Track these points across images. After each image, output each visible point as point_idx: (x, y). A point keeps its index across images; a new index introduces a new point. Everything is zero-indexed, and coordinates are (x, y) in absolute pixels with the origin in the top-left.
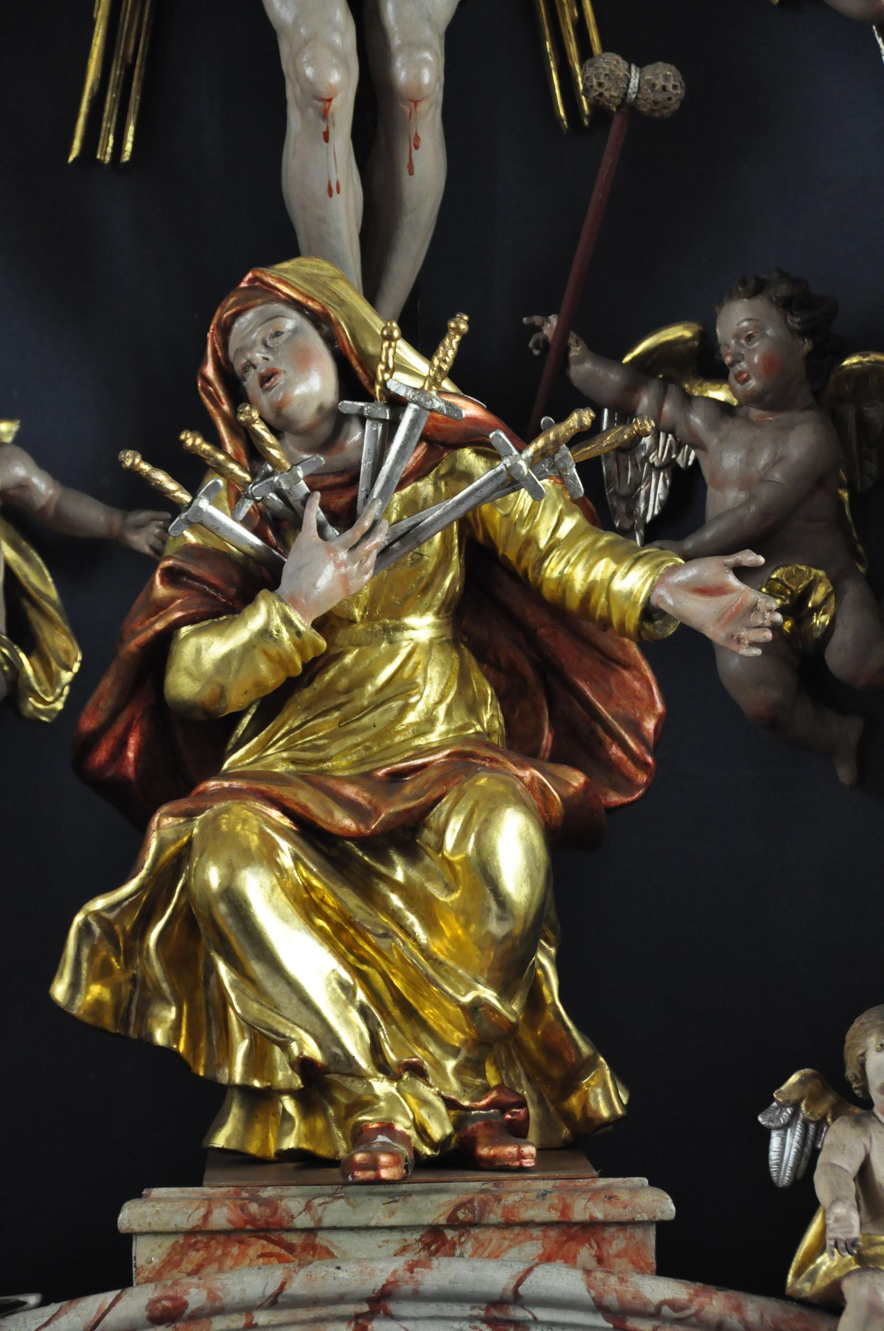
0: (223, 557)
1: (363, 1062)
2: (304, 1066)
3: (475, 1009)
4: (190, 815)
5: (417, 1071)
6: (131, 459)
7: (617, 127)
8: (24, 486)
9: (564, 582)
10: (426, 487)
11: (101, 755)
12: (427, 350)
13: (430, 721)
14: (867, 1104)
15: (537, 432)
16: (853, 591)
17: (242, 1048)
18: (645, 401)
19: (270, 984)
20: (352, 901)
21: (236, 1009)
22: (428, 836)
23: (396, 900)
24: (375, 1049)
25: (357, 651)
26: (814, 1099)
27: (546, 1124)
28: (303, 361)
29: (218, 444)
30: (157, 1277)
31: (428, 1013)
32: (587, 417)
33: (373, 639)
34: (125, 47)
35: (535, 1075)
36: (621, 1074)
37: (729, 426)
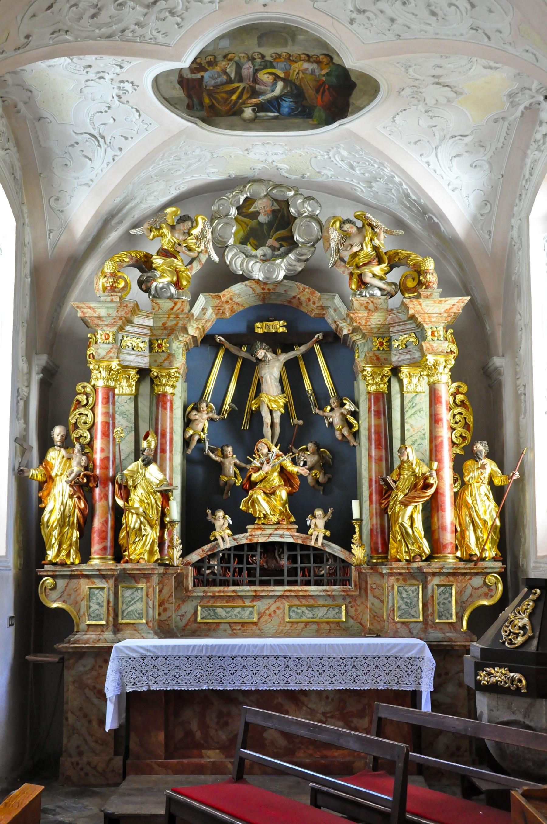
1: (269, 514)
2: (264, 514)
3: (280, 509)
5: (274, 515)
6: (248, 457)
10: (276, 460)
11: (245, 486)
17: (258, 513)
18: (300, 454)
20: (268, 499)
28: (264, 448)
34: (248, 417)
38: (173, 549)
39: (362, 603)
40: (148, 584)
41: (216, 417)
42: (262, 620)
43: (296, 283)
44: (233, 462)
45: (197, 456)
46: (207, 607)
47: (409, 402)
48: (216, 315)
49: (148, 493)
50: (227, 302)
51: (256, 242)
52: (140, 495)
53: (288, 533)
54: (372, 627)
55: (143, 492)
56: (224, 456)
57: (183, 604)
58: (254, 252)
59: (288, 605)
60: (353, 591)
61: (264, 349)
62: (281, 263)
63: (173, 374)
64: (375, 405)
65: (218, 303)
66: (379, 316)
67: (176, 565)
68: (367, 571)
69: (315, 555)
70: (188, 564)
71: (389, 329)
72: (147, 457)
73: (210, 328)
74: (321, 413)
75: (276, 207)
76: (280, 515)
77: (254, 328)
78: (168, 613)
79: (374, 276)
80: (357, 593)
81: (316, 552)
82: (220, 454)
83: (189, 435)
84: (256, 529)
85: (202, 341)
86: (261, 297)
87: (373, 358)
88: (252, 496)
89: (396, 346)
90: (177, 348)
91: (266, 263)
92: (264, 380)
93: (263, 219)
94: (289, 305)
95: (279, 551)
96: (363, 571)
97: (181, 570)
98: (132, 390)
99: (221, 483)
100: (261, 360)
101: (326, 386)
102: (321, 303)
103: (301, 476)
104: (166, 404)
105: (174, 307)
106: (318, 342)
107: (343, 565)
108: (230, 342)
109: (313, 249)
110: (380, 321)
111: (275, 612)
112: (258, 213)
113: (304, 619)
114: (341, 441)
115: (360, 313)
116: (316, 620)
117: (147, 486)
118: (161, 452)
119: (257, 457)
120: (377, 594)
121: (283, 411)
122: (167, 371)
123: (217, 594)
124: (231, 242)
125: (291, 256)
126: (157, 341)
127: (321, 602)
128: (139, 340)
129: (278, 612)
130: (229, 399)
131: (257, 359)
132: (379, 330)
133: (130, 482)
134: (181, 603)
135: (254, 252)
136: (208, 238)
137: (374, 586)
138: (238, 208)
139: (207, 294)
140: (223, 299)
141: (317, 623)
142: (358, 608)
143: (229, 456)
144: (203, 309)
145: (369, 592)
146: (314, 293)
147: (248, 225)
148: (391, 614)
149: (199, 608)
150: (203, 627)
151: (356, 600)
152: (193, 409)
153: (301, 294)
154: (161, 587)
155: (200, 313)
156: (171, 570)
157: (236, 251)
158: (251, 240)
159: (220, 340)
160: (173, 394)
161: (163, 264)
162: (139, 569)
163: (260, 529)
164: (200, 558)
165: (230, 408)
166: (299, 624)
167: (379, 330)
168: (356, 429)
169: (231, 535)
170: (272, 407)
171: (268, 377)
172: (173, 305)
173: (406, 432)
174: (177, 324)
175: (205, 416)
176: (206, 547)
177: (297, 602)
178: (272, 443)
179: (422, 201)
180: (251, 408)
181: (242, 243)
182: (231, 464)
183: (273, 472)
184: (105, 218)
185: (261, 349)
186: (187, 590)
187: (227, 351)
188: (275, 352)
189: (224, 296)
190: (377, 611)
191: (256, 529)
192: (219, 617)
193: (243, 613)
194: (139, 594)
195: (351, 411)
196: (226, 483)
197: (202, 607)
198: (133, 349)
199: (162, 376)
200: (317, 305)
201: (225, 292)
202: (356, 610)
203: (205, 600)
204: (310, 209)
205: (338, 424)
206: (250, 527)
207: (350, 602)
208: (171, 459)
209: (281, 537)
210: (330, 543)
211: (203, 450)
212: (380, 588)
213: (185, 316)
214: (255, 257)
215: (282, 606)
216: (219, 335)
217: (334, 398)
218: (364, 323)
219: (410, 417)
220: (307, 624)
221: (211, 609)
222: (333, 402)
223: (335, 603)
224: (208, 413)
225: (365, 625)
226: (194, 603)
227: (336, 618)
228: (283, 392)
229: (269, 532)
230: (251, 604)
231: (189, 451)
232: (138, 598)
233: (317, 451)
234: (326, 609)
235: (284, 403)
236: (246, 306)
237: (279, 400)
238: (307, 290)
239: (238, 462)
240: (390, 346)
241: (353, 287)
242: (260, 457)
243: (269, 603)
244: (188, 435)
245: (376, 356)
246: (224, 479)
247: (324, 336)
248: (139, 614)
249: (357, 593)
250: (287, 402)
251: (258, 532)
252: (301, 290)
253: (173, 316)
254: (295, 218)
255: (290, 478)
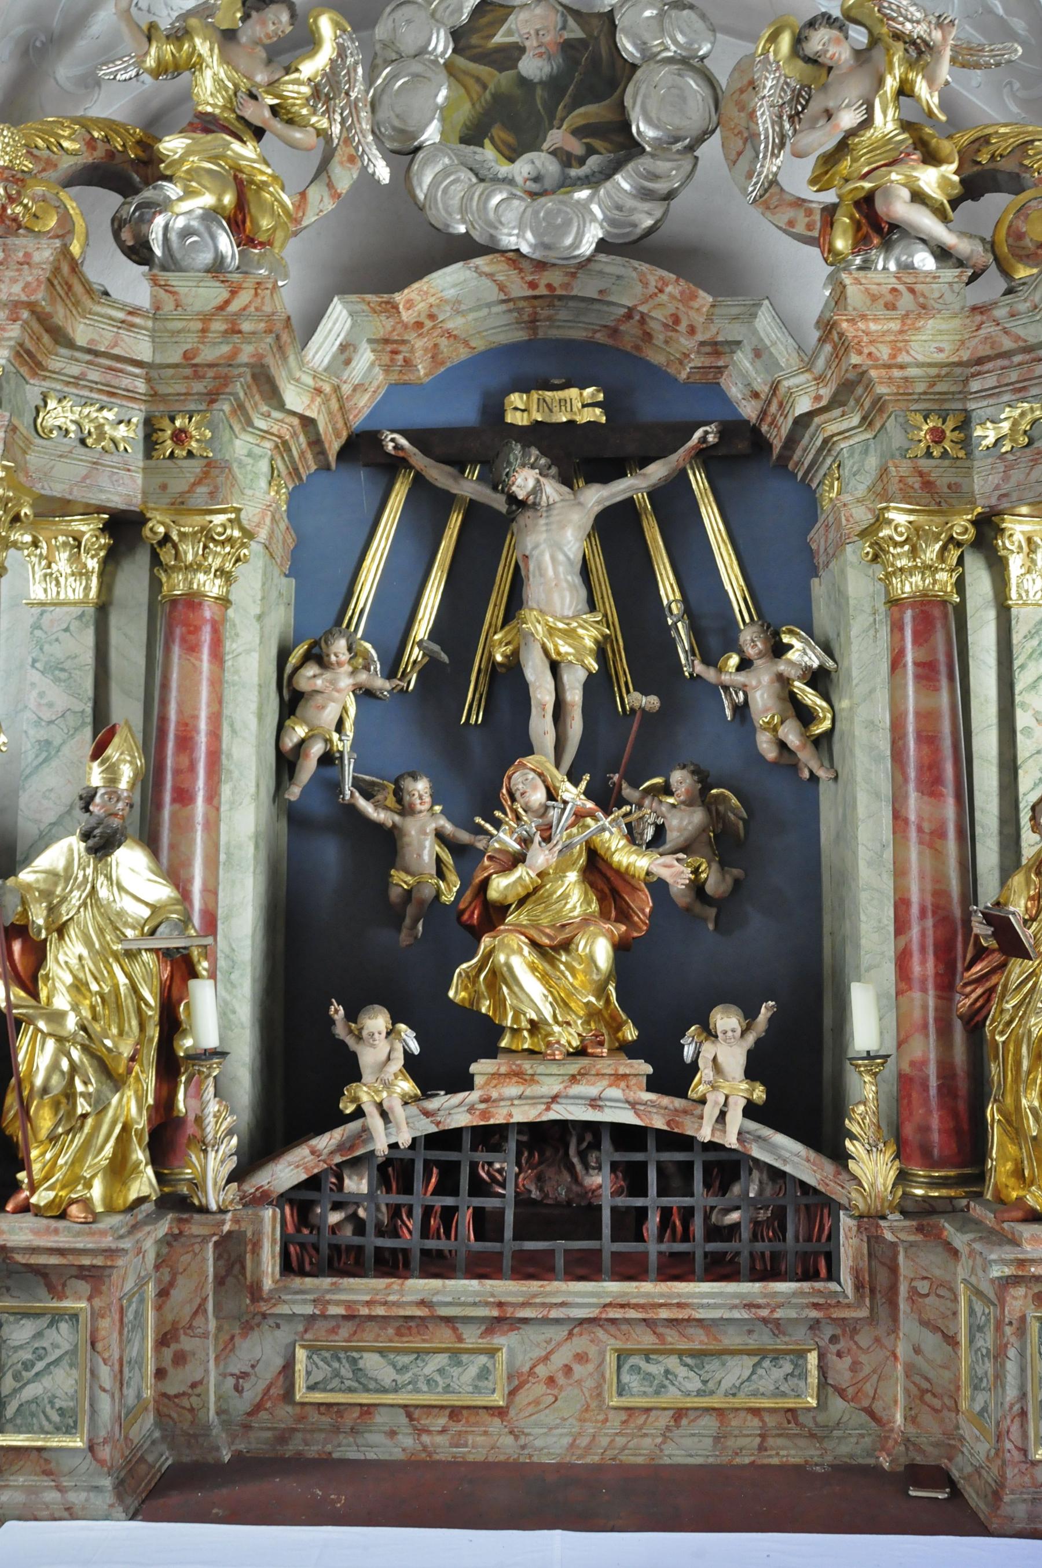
0: (508, 852)
1: (550, 1020)
2: (531, 1022)
4: (495, 937)
5: (568, 1024)
6: (478, 820)
7: (638, 715)
8: (443, 827)
9: (619, 862)
10: (574, 830)
11: (466, 917)
12: (576, 785)
13: (575, 907)
14: (716, 1037)
15: (612, 813)
16: (715, 866)
17: (510, 1014)
18: (647, 802)
19: (520, 994)
20: (548, 967)
21: (508, 1002)
22: (573, 946)
23: (562, 967)
24: (555, 1016)
25: (388, 70)
26: (699, 1035)
27: (611, 1041)
28: (535, 788)
29: (505, 814)
30: (482, 1088)
31: (572, 1005)
32: (628, 808)
33: (556, 880)
35: (608, 1025)
36: (635, 1025)
37: (674, 811)
38: (205, 1151)
39: (877, 1340)
40: (97, 1302)
41: (380, 683)
42: (523, 1398)
43: (636, 263)
44: (431, 827)
45: (319, 807)
46: (327, 1349)
47: (1029, 636)
48: (387, 369)
49: (103, 955)
50: (419, 325)
51: (510, 139)
52: (74, 962)
53: (615, 1092)
54: (912, 1430)
55: (85, 953)
56: (406, 810)
57: (244, 1335)
58: (504, 169)
59: (616, 1350)
60: (848, 1306)
61: (533, 467)
62: (590, 199)
63: (220, 529)
64: (916, 641)
65: (389, 328)
66: (940, 332)
67: (214, 1207)
68: (903, 1236)
69: (707, 1167)
70: (262, 1198)
71: (966, 381)
72: (99, 824)
73: (366, 411)
74: (710, 674)
75: (575, 32)
76: (587, 1022)
77: (502, 413)
78: (191, 1372)
79: (918, 197)
80: (863, 1313)
81: (711, 1156)
82: (391, 801)
83: (295, 740)
84: (507, 1075)
85: (344, 454)
86: (526, 318)
87: (910, 481)
88: (490, 954)
89: (990, 441)
90: (249, 455)
91: (543, 200)
92: (532, 566)
93: (532, 67)
94: (610, 342)
95: (580, 1142)
96: (889, 1236)
97: (236, 1221)
98: (87, 588)
99: (394, 894)
100: (522, 504)
101: (726, 593)
102: (714, 330)
103: (658, 887)
104: (196, 630)
105: (227, 302)
106: (705, 456)
107: (805, 1200)
108: (426, 451)
109: (687, 165)
110: (941, 350)
111: (568, 1370)
112: (521, 50)
113: (672, 1397)
114: (775, 764)
115: (876, 320)
116: (715, 1402)
117: (101, 932)
118: (174, 801)
119: (509, 819)
120: (930, 1315)
121: (594, 667)
122: (199, 520)
123: (364, 1311)
124: (431, 134)
125: (623, 181)
126: (172, 420)
127: (732, 1339)
128: (105, 413)
129: (578, 1370)
130: (422, 629)
131: (512, 499)
132: (933, 385)
133: (38, 917)
134: (237, 1331)
135: (504, 169)
136: (353, 95)
137: (923, 1287)
138: (457, 35)
139: (354, 298)
140: (407, 316)
141: (720, 1412)
142: (863, 1358)
143: (419, 807)
144: (343, 348)
145: (903, 1305)
146: (694, 297)
147: (485, 87)
148: (1015, 1428)
149: (301, 1354)
150: (314, 1416)
151: (855, 1331)
152: (308, 657)
153: (652, 303)
154: (167, 1278)
155: (334, 358)
156: (197, 1226)
157: (447, 161)
158: (497, 131)
159: (397, 447)
160: (224, 602)
161: (188, 152)
162: (60, 1252)
163: (518, 1075)
164: (304, 1177)
165: (424, 655)
166: (653, 1413)
167: (933, 385)
168: (827, 725)
169: (416, 1099)
170: (559, 654)
171: (547, 557)
172: (225, 295)
173: (1019, 737)
174: (235, 352)
175: (346, 682)
176: (326, 1142)
177: (648, 1340)
178: (558, 765)
179: (827, 293)
180: (491, 656)
181: (465, 140)
182: (425, 834)
183: (561, 870)
184: (20, 30)
185: (523, 465)
186: (255, 1291)
187: (420, 482)
188: (567, 481)
189: (410, 304)
190: (931, 1375)
191: (507, 1075)
192: (372, 1385)
193: (455, 1371)
194: (63, 1337)
195: (808, 668)
196: (409, 893)
197: (313, 1350)
198: (83, 442)
199: (183, 535)
200: (700, 337)
201: (412, 292)
202: (855, 1367)
203: (321, 1326)
204: (680, 38)
205: (767, 710)
206: (481, 1068)
207: (834, 1339)
208: (212, 826)
209: (594, 1107)
210: (766, 1132)
211: (337, 787)
212: (942, 1292)
213: (262, 325)
214: (509, 181)
215: (593, 1351)
216: (393, 431)
217: (756, 628)
218: (886, 357)
219: (1033, 686)
220: (679, 1414)
221: (342, 1355)
222: (752, 641)
223: (780, 1344)
224: (354, 673)
225: (885, 1419)
226: (284, 1335)
227: (784, 1395)
228: (592, 607)
229: (551, 1086)
230: (483, 1343)
231: (294, 793)
232: (58, 1353)
233: (702, 797)
234: (749, 1362)
235: (597, 642)
236: (480, 344)
237: (580, 631)
238: (669, 289)
239: (449, 827)
240: (966, 443)
241: (841, 244)
242: (518, 818)
243: (548, 1342)
244: (289, 742)
245: (921, 474)
246: (401, 880)
247: (722, 434)
248: (61, 1411)
249: (863, 1313)
250: (606, 637)
251: (512, 1090)
252: (652, 289)
253: (218, 326)
254: (634, 67)
255: (619, 884)
